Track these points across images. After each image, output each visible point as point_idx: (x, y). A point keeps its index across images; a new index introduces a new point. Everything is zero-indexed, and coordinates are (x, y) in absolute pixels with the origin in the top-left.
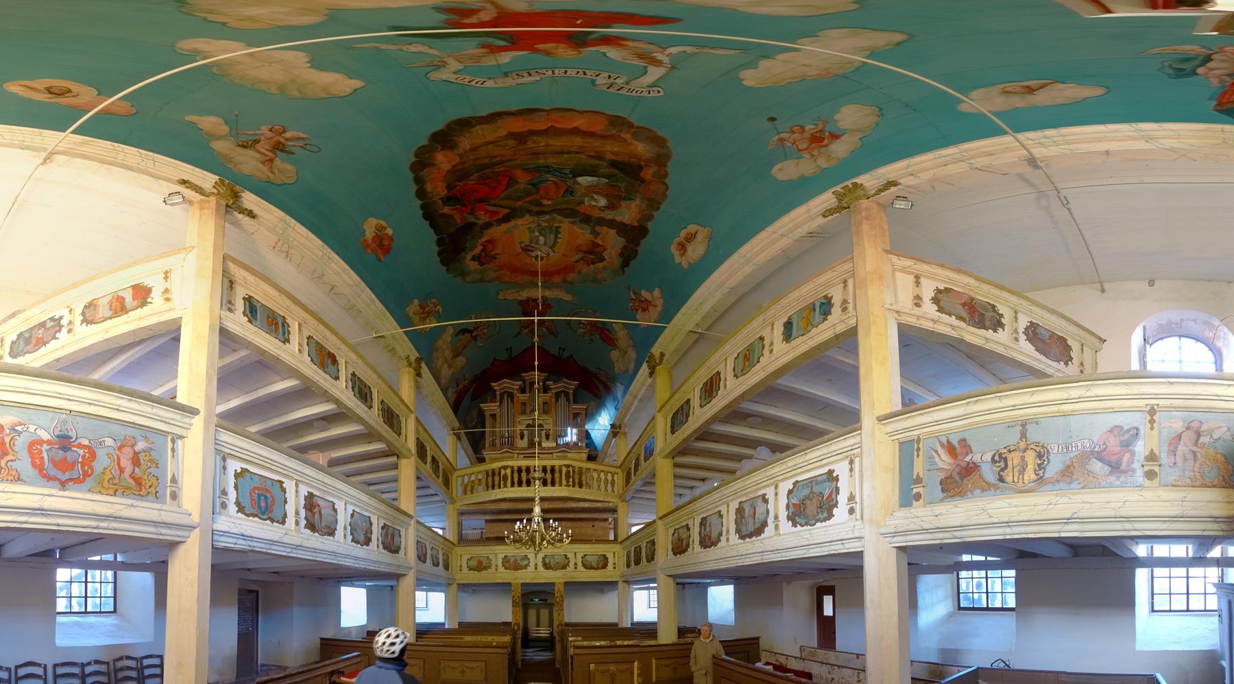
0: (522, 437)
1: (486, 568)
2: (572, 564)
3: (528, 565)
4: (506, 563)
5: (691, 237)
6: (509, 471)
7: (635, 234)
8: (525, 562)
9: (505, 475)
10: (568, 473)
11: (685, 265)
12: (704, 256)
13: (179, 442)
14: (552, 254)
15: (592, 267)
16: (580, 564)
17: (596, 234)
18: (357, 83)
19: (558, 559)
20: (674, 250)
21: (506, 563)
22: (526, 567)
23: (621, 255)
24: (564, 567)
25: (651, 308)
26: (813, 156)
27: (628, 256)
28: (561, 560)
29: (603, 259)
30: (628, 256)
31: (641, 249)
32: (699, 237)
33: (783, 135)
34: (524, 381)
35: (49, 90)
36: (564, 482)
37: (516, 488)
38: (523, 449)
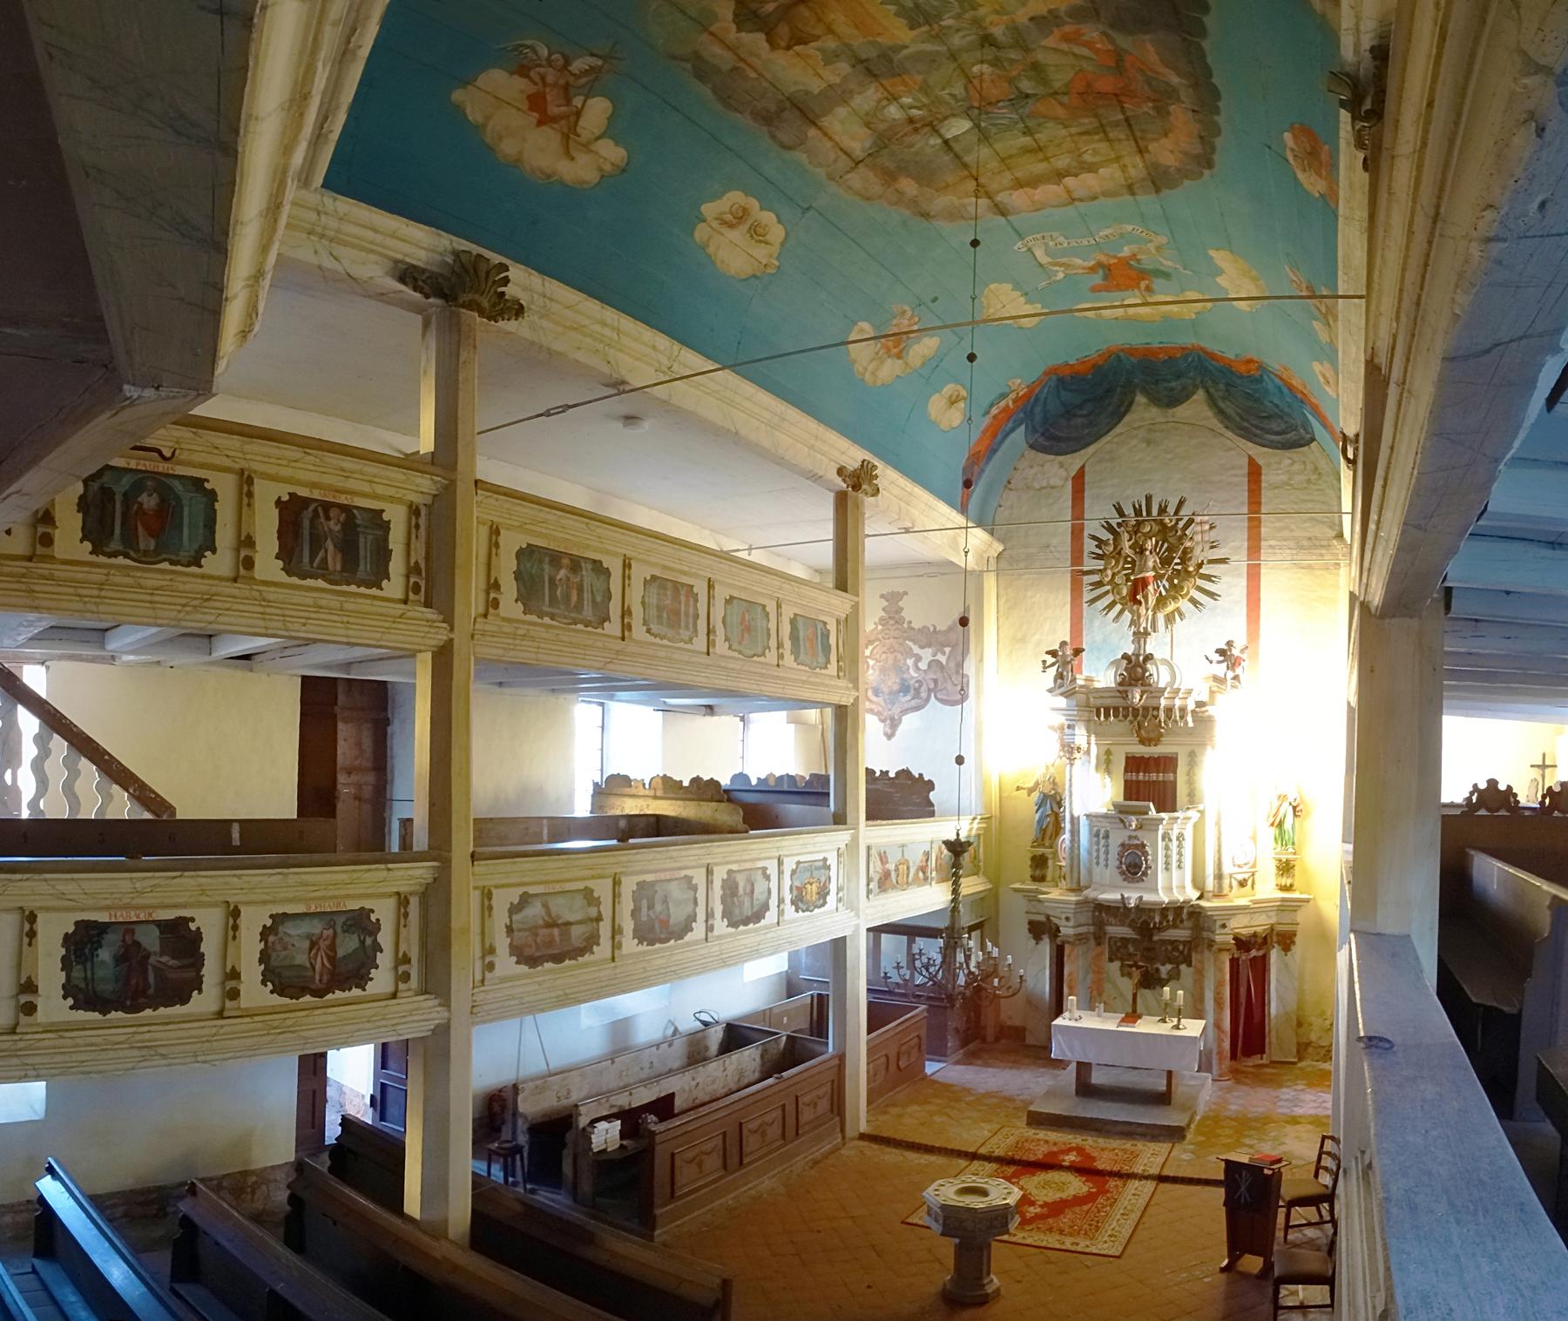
5: (757, 233)
11: (701, 232)
13: (1097, 1078)
18: (1212, 253)
20: (735, 198)
32: (761, 252)
35: (984, 1193)
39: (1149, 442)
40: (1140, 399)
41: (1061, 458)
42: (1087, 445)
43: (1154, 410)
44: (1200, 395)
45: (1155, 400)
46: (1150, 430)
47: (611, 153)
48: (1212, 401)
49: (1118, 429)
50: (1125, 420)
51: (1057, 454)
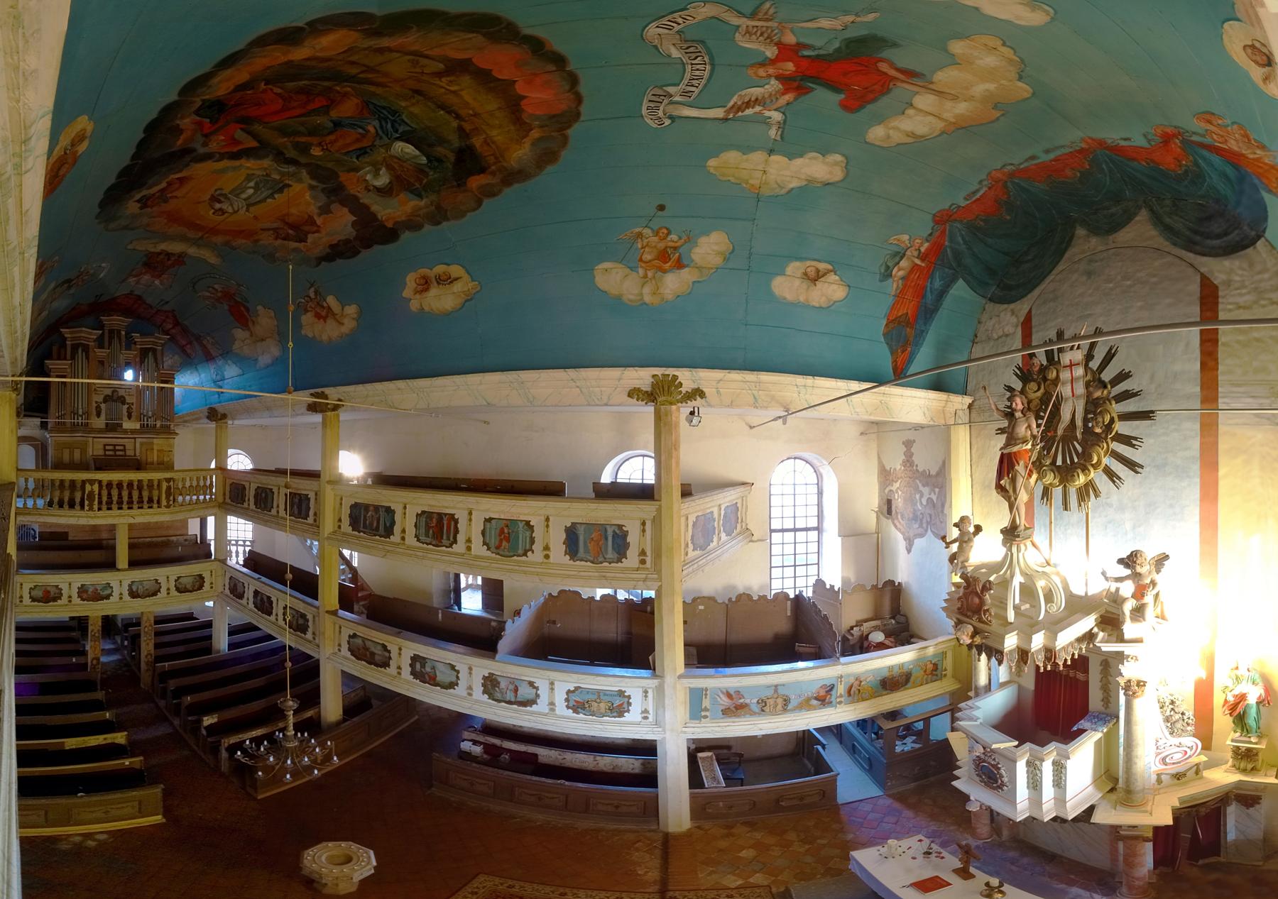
0: (98, 415)
1: (55, 600)
2: (163, 590)
3: (111, 595)
4: (82, 592)
6: (96, 487)
7: (374, 233)
8: (109, 592)
9: (92, 493)
10: (169, 488)
11: (414, 305)
12: (447, 314)
14: (242, 212)
15: (279, 242)
16: (173, 589)
17: (325, 210)
19: (147, 585)
20: (411, 280)
21: (82, 592)
22: (107, 597)
23: (332, 246)
24: (155, 594)
25: (330, 321)
26: (645, 276)
27: (340, 251)
28: (150, 586)
29: (303, 240)
30: (340, 251)
31: (365, 254)
32: (457, 287)
33: (647, 232)
34: (101, 327)
36: (164, 502)
37: (105, 512)
38: (100, 431)
39: (1089, 274)
40: (1080, 232)
41: (1012, 306)
42: (1035, 287)
43: (1094, 241)
44: (1143, 215)
45: (1095, 230)
46: (1091, 261)
47: (351, 310)
48: (1157, 220)
49: (1060, 267)
50: (1067, 255)
51: (1009, 302)
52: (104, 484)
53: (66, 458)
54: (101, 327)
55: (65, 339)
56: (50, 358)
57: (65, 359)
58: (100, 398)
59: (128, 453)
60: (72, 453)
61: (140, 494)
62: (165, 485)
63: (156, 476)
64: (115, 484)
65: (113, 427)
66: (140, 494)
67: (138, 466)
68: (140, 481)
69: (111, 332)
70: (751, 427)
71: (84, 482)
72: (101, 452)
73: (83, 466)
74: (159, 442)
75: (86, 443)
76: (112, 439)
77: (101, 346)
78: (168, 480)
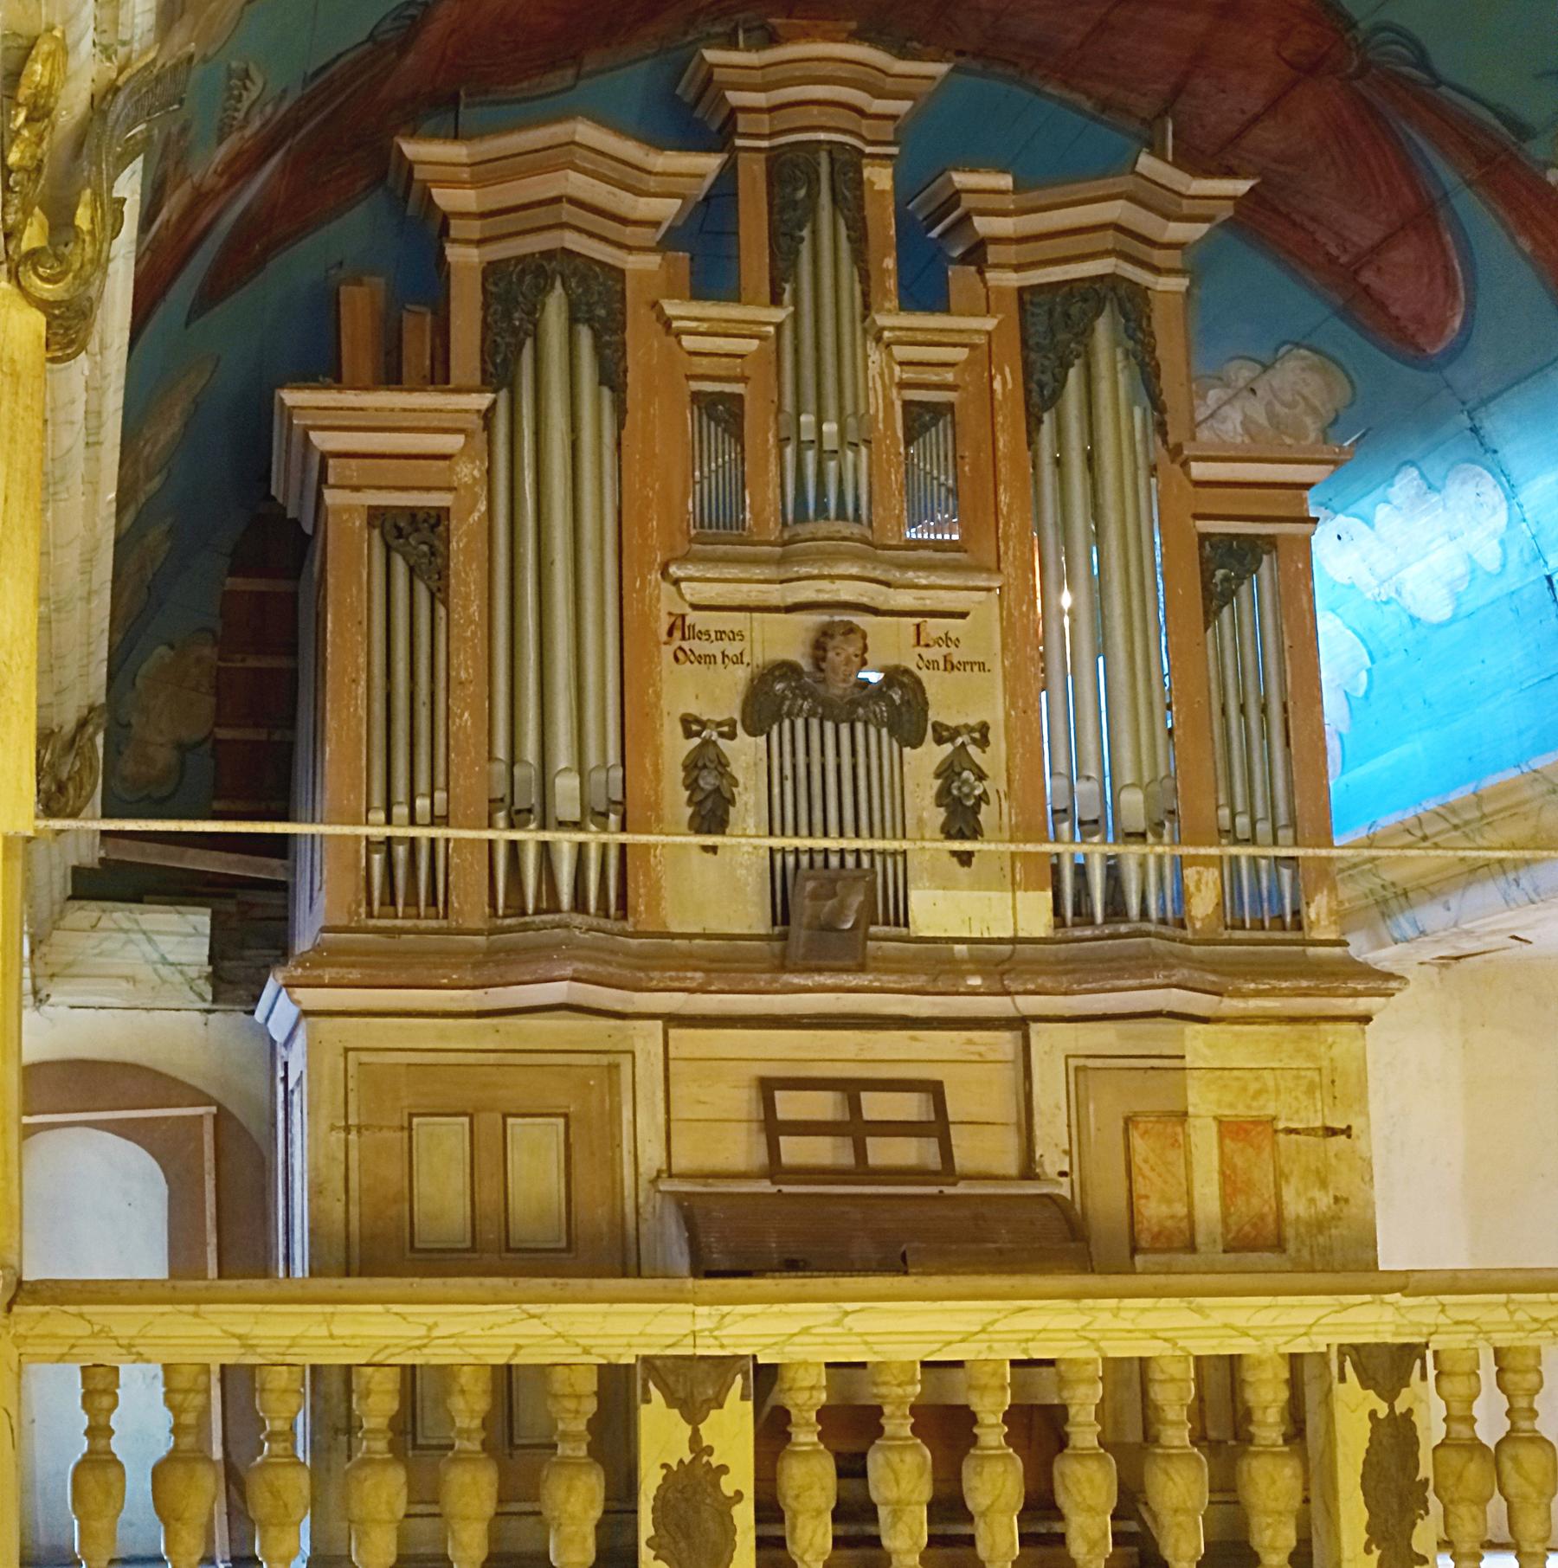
0: (712, 814)
6: (732, 1430)
9: (694, 1483)
10: (1395, 1437)
38: (722, 960)
52: (806, 1397)
53: (443, 1194)
54: (695, 119)
55: (441, 225)
56: (325, 368)
57: (439, 377)
58: (718, 693)
59: (970, 1151)
60: (487, 1161)
61: (1227, 1492)
62: (1353, 1412)
63: (1265, 1326)
64: (898, 1399)
65: (826, 920)
66: (1227, 1492)
67: (1049, 1237)
68: (1132, 1379)
69: (787, 169)
70: (1128, 1121)
71: (618, 1388)
72: (738, 1149)
73: (590, 1251)
74: (1228, 1058)
75: (610, 1070)
76: (825, 1034)
77: (712, 275)
78: (1388, 1366)
